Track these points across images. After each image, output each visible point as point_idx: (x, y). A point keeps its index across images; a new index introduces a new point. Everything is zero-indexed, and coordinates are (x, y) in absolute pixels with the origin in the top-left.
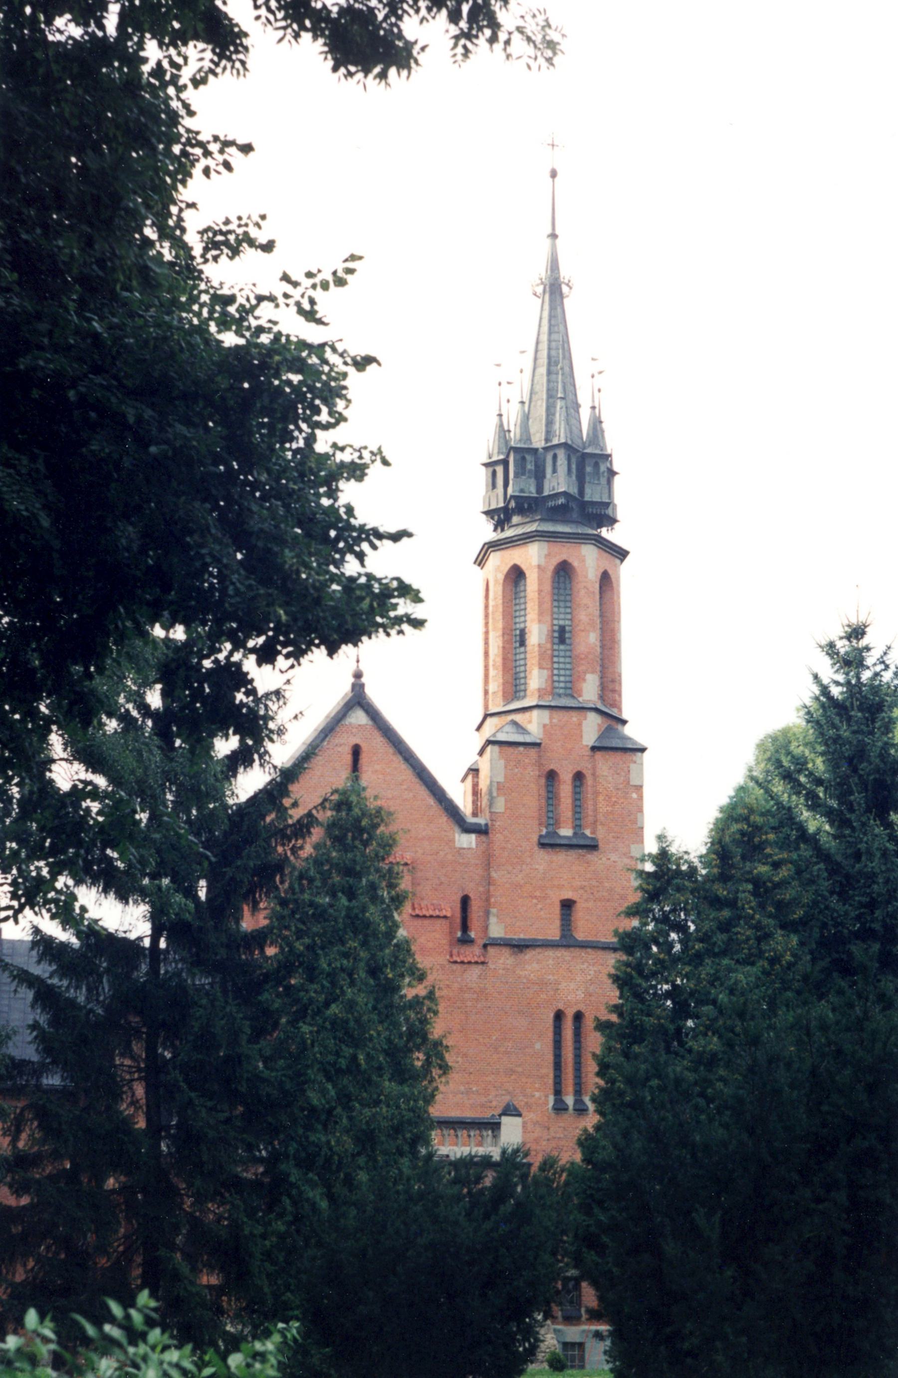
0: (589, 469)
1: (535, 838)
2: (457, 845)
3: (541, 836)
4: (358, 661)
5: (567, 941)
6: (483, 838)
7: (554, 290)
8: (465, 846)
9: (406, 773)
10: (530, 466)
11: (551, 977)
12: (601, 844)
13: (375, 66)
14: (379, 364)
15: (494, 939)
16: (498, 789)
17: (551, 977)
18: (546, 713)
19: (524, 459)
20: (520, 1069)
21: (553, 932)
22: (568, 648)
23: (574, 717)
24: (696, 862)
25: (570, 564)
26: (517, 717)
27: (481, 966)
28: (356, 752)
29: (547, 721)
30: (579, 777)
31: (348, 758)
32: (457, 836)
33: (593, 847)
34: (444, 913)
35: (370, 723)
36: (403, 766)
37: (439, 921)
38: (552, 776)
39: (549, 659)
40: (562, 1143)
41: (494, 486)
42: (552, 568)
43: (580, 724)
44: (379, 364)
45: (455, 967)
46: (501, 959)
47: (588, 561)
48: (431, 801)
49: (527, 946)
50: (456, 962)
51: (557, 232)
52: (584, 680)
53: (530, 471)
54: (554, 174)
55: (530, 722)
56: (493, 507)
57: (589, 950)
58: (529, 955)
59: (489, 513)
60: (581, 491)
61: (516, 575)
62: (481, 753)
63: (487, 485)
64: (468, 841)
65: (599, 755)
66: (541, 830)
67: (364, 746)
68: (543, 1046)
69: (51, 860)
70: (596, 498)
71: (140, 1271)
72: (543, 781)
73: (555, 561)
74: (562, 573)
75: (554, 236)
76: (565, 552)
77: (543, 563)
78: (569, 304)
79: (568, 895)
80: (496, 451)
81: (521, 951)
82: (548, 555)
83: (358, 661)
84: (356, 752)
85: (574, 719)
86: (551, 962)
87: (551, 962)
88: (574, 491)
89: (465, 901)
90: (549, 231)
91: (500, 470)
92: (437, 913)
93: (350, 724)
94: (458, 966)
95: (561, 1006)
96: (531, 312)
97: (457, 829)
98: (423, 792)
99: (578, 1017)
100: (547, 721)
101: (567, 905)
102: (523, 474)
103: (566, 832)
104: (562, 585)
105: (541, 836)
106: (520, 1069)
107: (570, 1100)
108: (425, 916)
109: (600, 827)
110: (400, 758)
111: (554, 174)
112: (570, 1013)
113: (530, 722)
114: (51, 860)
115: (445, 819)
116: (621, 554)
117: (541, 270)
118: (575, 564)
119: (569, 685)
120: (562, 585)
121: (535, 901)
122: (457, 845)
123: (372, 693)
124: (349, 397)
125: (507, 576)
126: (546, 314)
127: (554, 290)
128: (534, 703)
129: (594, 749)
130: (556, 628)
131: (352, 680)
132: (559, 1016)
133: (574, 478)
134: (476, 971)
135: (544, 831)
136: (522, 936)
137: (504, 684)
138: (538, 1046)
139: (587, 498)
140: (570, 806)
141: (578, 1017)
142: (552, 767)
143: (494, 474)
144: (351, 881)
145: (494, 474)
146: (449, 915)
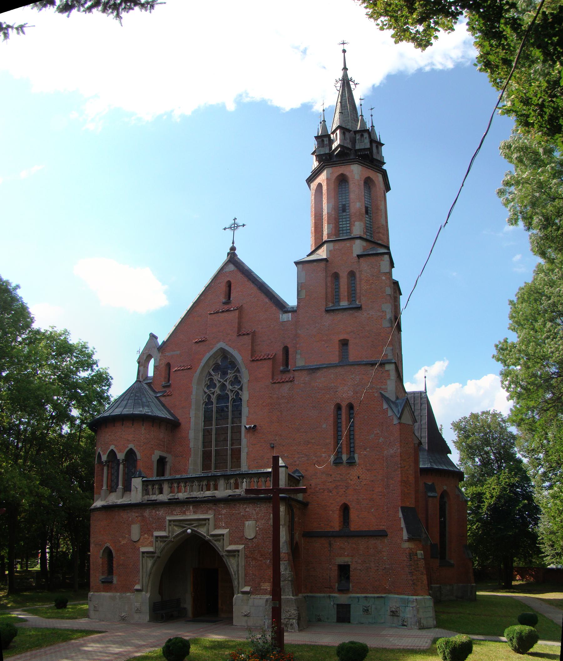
2: (281, 320)
5: (344, 361)
9: (254, 289)
11: (333, 385)
12: (363, 307)
15: (299, 367)
17: (333, 385)
20: (313, 441)
21: (334, 358)
23: (348, 244)
24: (504, 368)
25: (345, 175)
27: (289, 384)
30: (352, 274)
33: (359, 308)
35: (236, 269)
40: (339, 484)
42: (334, 178)
43: (351, 247)
45: (275, 386)
46: (302, 378)
49: (318, 369)
50: (275, 383)
57: (356, 367)
58: (319, 374)
65: (362, 260)
67: (232, 281)
68: (327, 426)
71: (293, 612)
79: (342, 337)
81: (314, 373)
85: (348, 245)
86: (332, 376)
87: (332, 376)
89: (286, 350)
93: (226, 272)
94: (277, 385)
95: (338, 401)
98: (262, 296)
99: (351, 407)
101: (344, 343)
103: (344, 304)
106: (313, 441)
107: (345, 457)
108: (257, 360)
109: (362, 297)
110: (251, 282)
112: (344, 405)
115: (274, 308)
117: (340, 75)
121: (324, 343)
122: (281, 320)
124: (94, 10)
129: (359, 256)
130: (347, 211)
132: (338, 407)
134: (287, 386)
136: (315, 363)
138: (324, 426)
140: (341, 287)
141: (351, 407)
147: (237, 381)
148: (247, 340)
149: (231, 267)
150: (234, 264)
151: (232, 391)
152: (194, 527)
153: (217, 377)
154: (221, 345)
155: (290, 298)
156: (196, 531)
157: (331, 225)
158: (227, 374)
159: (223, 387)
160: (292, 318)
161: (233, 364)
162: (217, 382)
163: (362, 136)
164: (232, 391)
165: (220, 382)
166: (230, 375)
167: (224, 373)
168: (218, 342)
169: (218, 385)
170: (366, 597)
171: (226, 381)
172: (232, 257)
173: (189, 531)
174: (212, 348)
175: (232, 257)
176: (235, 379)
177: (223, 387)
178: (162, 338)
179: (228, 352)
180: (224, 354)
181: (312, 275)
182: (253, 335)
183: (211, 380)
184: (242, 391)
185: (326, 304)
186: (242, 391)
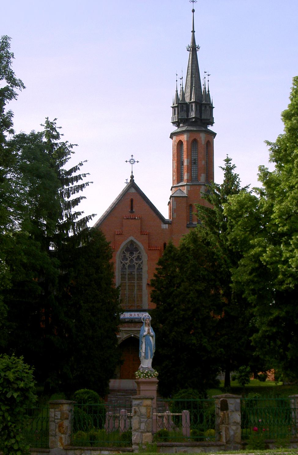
0: (203, 108)
1: (185, 225)
3: (187, 224)
4: (132, 173)
6: (170, 225)
7: (194, 49)
8: (165, 228)
10: (185, 109)
13: (34, 376)
14: (85, 198)
16: (174, 211)
18: (189, 187)
19: (183, 106)
22: (197, 165)
26: (181, 188)
28: (132, 201)
29: (189, 189)
31: (129, 203)
32: (162, 225)
34: (158, 249)
35: (136, 192)
36: (146, 204)
37: (156, 251)
38: (191, 206)
39: (190, 170)
41: (175, 114)
42: (191, 141)
44: (85, 198)
47: (202, 137)
48: (155, 215)
51: (195, 30)
52: (201, 176)
53: (185, 110)
54: (193, 11)
55: (184, 189)
56: (174, 121)
59: (173, 123)
60: (201, 116)
61: (180, 143)
62: (170, 199)
63: (173, 114)
64: (165, 226)
66: (187, 223)
69: (89, 237)
70: (205, 118)
72: (188, 208)
73: (192, 139)
74: (195, 142)
75: (193, 32)
76: (195, 136)
77: (188, 140)
78: (198, 53)
80: (175, 103)
82: (190, 137)
83: (132, 173)
84: (132, 201)
88: (198, 116)
90: (192, 30)
91: (176, 109)
92: (156, 248)
96: (187, 55)
97: (162, 223)
98: (152, 212)
100: (189, 189)
102: (183, 111)
104: (195, 146)
105: (187, 224)
111: (193, 11)
113: (184, 189)
114: (89, 237)
116: (214, 134)
117: (190, 43)
118: (198, 139)
119: (197, 177)
120: (195, 146)
123: (136, 182)
125: (178, 144)
126: (191, 58)
127: (194, 49)
128: (185, 184)
131: (91, 214)
133: (198, 111)
135: (188, 223)
137: (177, 177)
139: (203, 118)
142: (191, 203)
143: (175, 110)
144: (287, 248)
145: (175, 110)
146: (160, 249)
147: (139, 258)
148: (145, 237)
149: (133, 190)
150: (134, 188)
151: (137, 264)
152: (135, 334)
153: (128, 255)
154: (131, 238)
155: (165, 213)
156: (136, 336)
157: (189, 174)
158: (134, 254)
159: (132, 261)
160: (168, 228)
161: (136, 249)
162: (128, 258)
163: (206, 107)
164: (137, 264)
165: (130, 258)
166: (135, 255)
167: (132, 253)
168: (130, 236)
169: (129, 259)
170: (201, 436)
171: (133, 257)
172: (132, 185)
173: (132, 335)
174: (127, 239)
175: (132, 185)
176: (138, 257)
177: (132, 261)
178: (88, 222)
179: (135, 243)
180: (132, 242)
181: (180, 205)
182: (148, 234)
183: (125, 256)
184: (142, 264)
185: (187, 223)
186: (142, 264)
